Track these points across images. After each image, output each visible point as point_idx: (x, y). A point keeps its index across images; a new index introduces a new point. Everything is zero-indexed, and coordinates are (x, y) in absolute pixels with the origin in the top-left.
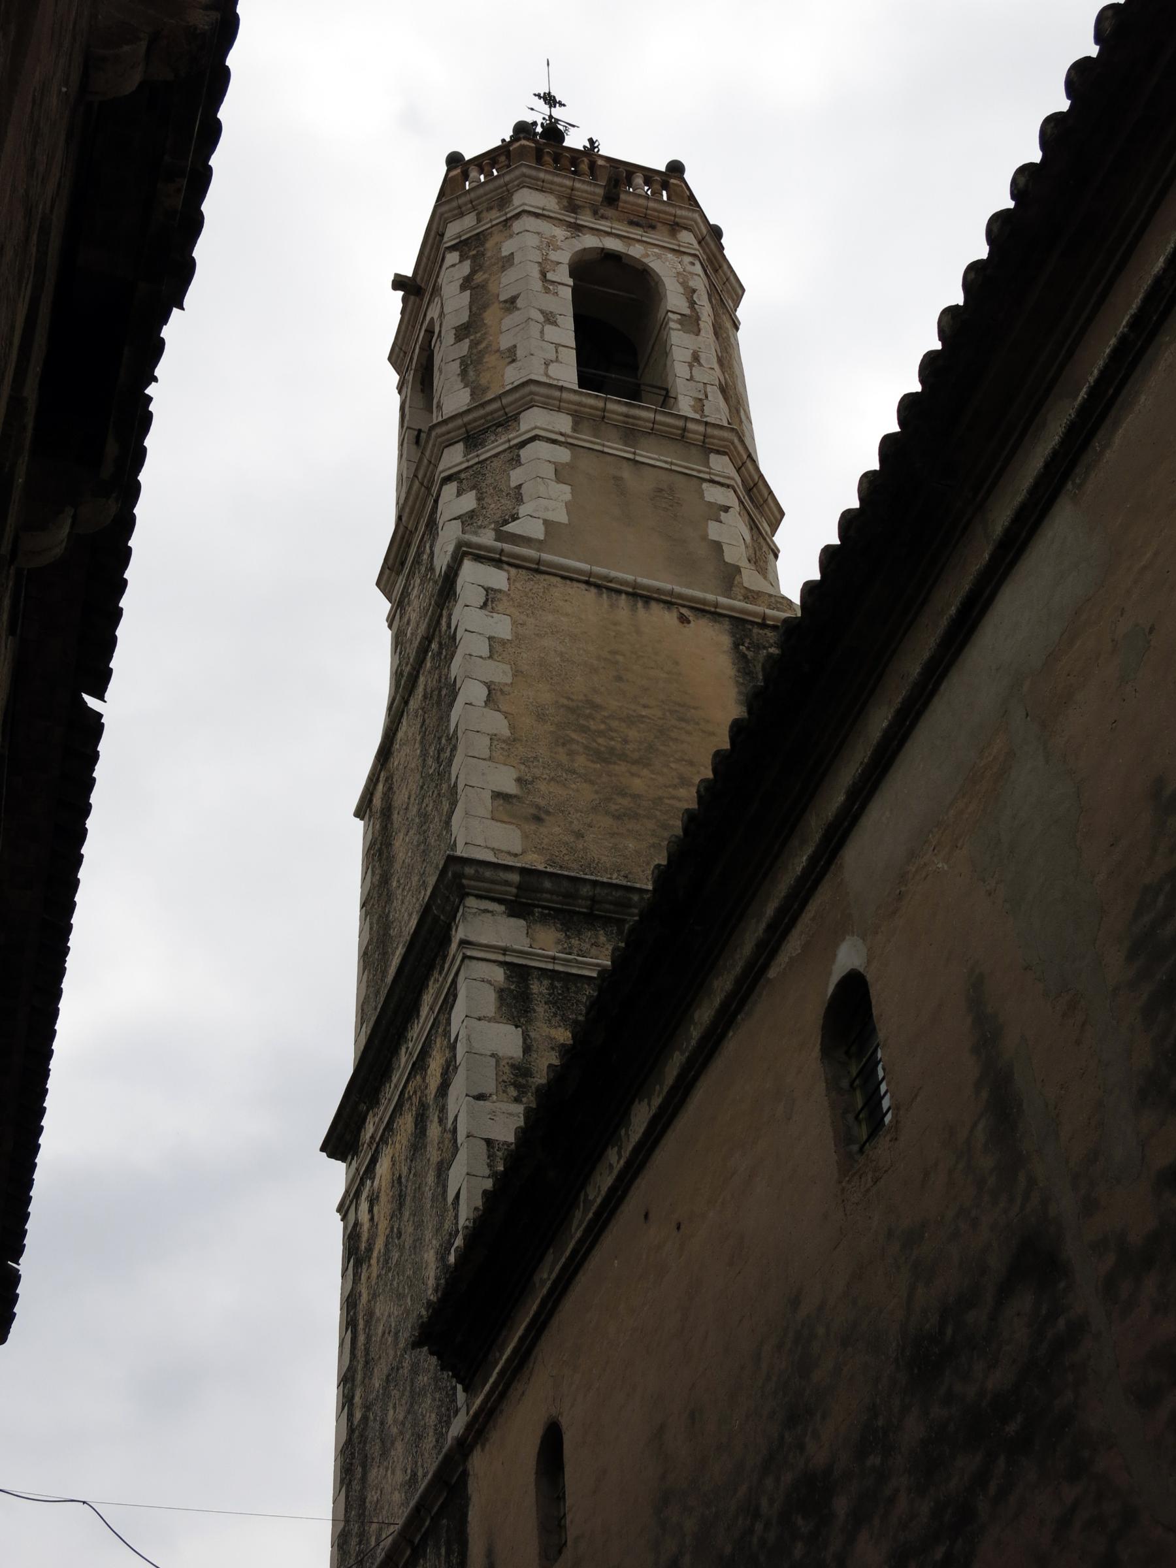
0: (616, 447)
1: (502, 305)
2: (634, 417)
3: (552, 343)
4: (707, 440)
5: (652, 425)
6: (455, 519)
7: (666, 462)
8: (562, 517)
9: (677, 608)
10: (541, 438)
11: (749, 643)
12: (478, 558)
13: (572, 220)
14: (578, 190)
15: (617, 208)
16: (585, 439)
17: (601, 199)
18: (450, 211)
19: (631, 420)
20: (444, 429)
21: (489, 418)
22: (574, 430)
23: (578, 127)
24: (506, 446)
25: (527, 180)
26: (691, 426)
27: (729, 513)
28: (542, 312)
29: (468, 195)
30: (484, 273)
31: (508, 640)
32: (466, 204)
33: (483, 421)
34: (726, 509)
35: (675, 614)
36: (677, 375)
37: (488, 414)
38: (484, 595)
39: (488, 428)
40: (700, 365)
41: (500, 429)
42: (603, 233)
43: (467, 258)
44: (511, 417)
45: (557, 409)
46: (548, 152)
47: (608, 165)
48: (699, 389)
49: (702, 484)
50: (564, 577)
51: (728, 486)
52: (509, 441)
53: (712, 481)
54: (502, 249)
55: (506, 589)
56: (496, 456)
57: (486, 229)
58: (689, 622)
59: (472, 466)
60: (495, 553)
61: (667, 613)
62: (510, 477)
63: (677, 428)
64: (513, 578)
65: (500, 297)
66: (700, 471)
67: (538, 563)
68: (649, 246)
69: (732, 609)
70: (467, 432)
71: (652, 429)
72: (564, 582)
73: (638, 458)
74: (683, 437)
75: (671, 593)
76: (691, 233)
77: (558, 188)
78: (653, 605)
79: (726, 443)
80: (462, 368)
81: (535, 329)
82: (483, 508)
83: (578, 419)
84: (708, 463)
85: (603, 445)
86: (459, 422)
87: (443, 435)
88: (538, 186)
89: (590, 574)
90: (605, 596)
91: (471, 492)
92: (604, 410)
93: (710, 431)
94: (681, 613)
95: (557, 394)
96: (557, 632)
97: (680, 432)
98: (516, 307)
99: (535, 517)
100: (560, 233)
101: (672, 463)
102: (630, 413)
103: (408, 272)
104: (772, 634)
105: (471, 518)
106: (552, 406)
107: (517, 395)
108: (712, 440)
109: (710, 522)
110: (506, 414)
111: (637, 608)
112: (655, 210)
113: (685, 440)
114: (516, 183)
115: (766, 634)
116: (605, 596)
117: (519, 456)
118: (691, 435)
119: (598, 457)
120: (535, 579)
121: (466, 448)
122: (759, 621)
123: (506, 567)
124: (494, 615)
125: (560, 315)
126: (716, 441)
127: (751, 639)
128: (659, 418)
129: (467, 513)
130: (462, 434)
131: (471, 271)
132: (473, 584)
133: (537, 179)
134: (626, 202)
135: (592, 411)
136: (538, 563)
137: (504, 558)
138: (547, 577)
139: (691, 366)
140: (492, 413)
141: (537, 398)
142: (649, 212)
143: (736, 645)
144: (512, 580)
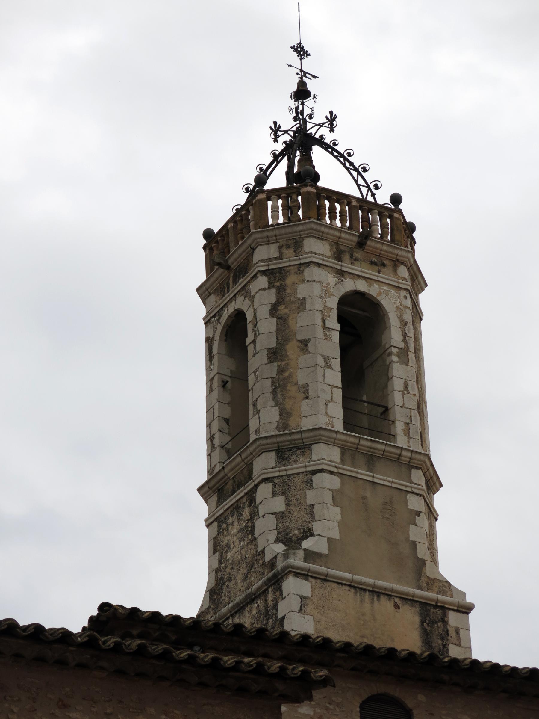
0: (363, 474)
1: (298, 344)
2: (374, 449)
3: (329, 385)
4: (411, 461)
5: (382, 453)
6: (272, 514)
7: (389, 481)
8: (335, 534)
9: (394, 598)
10: (325, 471)
11: (429, 620)
12: (297, 575)
13: (339, 267)
14: (343, 238)
15: (364, 250)
16: (348, 470)
17: (355, 244)
18: (262, 238)
19: (372, 450)
20: (265, 442)
21: (293, 442)
22: (342, 461)
23: (318, 78)
24: (303, 470)
25: (314, 232)
26: (404, 453)
27: (420, 517)
28: (324, 357)
29: (274, 231)
30: (286, 308)
31: (312, 634)
32: (272, 237)
33: (289, 443)
34: (419, 514)
35: (392, 603)
36: (396, 404)
37: (292, 440)
38: (300, 602)
39: (292, 448)
40: (409, 393)
41: (299, 452)
42: (356, 276)
43: (274, 286)
44: (306, 445)
45: (332, 444)
46: (323, 196)
47: (358, 205)
48: (407, 414)
49: (407, 495)
50: (338, 583)
51: (420, 495)
52: (306, 467)
53: (413, 493)
54: (298, 291)
55: (310, 596)
56: (297, 474)
57: (287, 267)
58: (399, 608)
59: (282, 476)
60: (305, 571)
61: (388, 602)
62: (306, 495)
63: (396, 454)
64: (313, 587)
65: (297, 336)
66: (406, 486)
67: (326, 576)
68: (383, 285)
69: (422, 597)
70: (278, 447)
71: (382, 455)
72: (339, 586)
73: (376, 480)
74: (398, 459)
75: (392, 590)
76: (405, 267)
77: (331, 237)
78: (383, 598)
79: (421, 463)
80: (273, 388)
81: (320, 371)
82: (290, 513)
83: (344, 450)
84: (410, 477)
85: (357, 473)
86: (274, 440)
87: (264, 445)
88: (319, 235)
89: (352, 581)
90: (358, 594)
91: (281, 497)
92: (358, 444)
93: (414, 456)
94: (395, 602)
95: (334, 435)
96: (336, 625)
97: (397, 456)
98: (307, 350)
99: (323, 537)
100: (331, 279)
101: (392, 482)
102: (372, 446)
104: (440, 612)
105: (282, 517)
106: (330, 442)
107: (311, 434)
108: (414, 461)
109: (410, 525)
110: (303, 443)
111: (374, 601)
112: (386, 252)
113: (399, 461)
114: (307, 232)
115: (437, 612)
116: (358, 594)
117: (311, 480)
118: (403, 458)
119: (354, 482)
120: (324, 586)
121: (278, 458)
122: (434, 603)
123: (310, 579)
124: (306, 616)
125: (333, 358)
126: (416, 462)
127: (429, 617)
128: (388, 449)
129: (279, 513)
130: (275, 447)
131: (277, 301)
132: (294, 594)
133: (319, 231)
134: (370, 246)
135: (352, 445)
136: (326, 576)
137: (309, 574)
138: (330, 583)
139: (403, 394)
140: (295, 440)
141: (323, 438)
142: (382, 252)
143: (422, 622)
144: (313, 589)
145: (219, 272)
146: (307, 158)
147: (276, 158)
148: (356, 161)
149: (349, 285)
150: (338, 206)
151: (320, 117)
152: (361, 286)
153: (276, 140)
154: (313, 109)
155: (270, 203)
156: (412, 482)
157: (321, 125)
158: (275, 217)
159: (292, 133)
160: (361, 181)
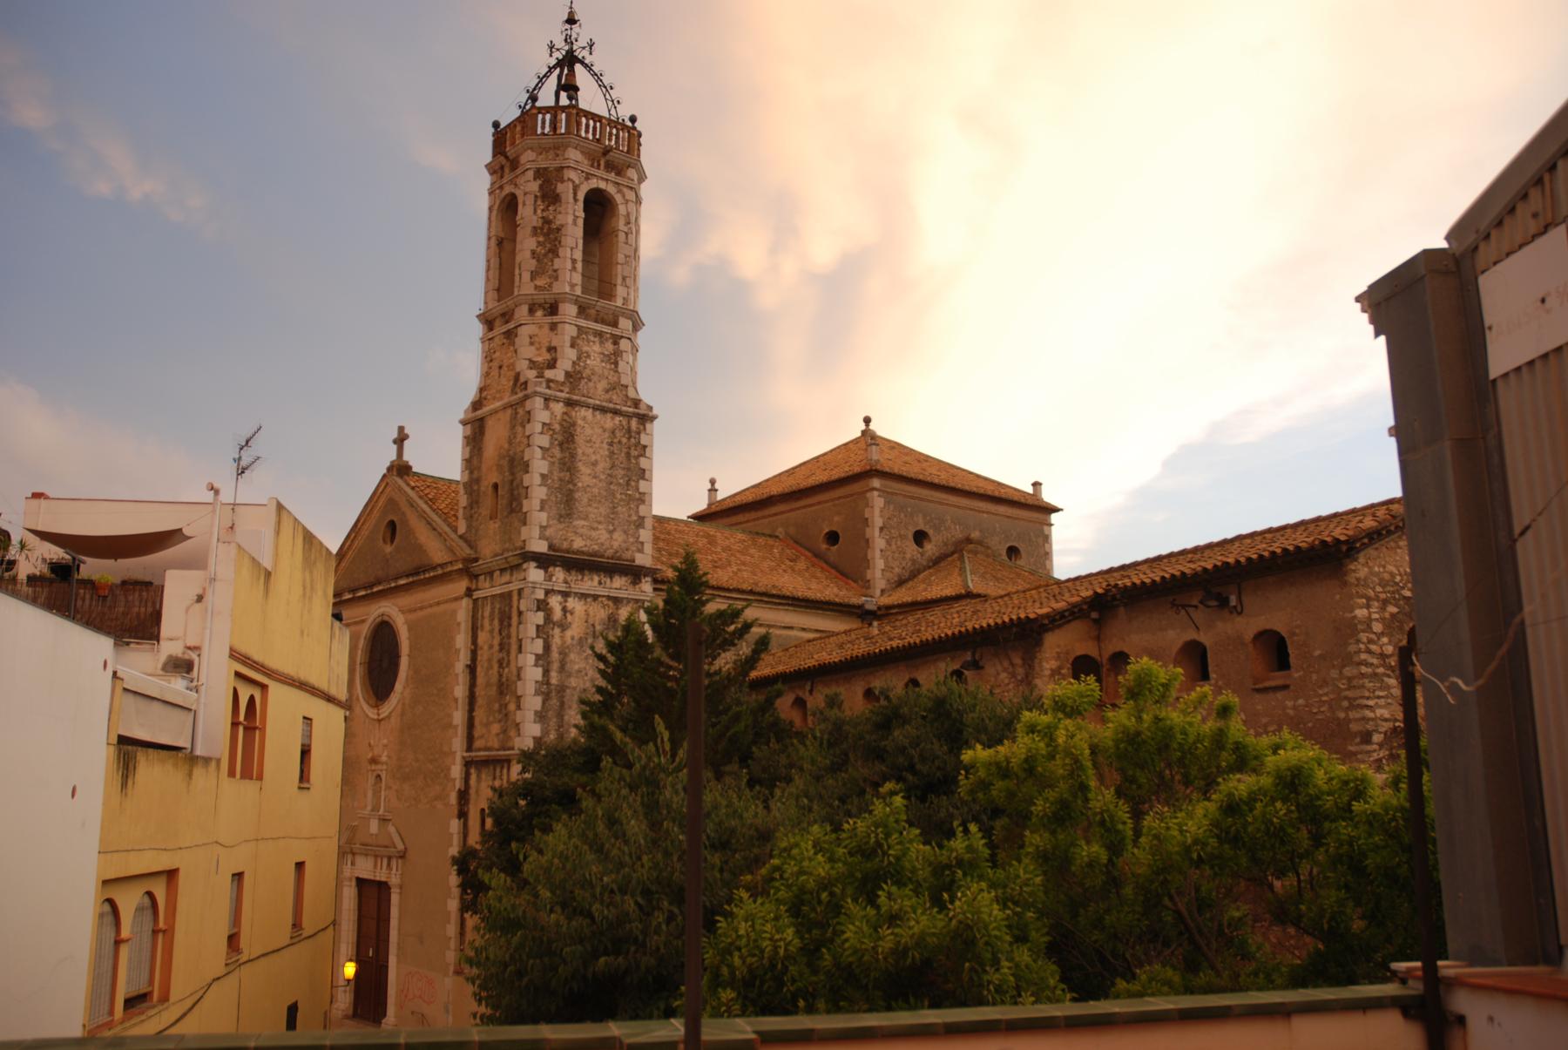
145: (502, 159)
146: (572, 72)
147: (551, 70)
148: (606, 81)
149: (594, 183)
150: (591, 122)
151: (583, 42)
152: (602, 185)
153: (551, 56)
154: (578, 34)
155: (540, 116)
156: (576, 325)
157: (584, 48)
158: (543, 127)
159: (564, 53)
160: (608, 96)
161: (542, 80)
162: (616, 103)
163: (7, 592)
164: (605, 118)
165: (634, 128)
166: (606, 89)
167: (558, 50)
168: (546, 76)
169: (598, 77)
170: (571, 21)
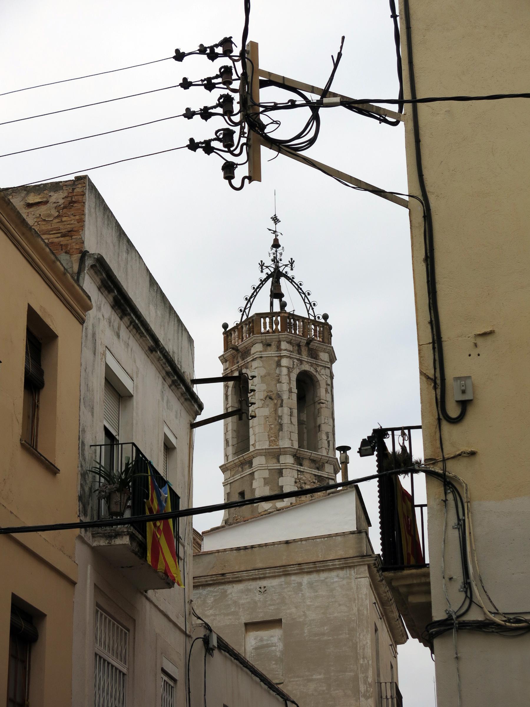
103: (231, 39)
147: (263, 282)
148: (304, 289)
151: (285, 260)
153: (262, 272)
155: (262, 320)
157: (286, 265)
158: (265, 327)
160: (306, 301)
161: (257, 290)
162: (312, 305)
163: (33, 700)
164: (306, 318)
165: (327, 324)
166: (305, 295)
167: (267, 267)
168: (259, 287)
169: (299, 288)
170: (276, 245)
